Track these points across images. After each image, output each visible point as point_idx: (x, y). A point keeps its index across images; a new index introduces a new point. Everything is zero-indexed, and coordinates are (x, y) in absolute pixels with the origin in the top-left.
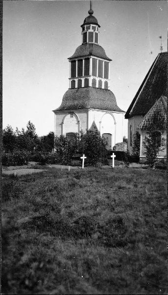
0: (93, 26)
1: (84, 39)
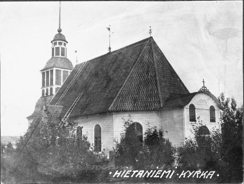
0: (59, 42)
1: (52, 51)
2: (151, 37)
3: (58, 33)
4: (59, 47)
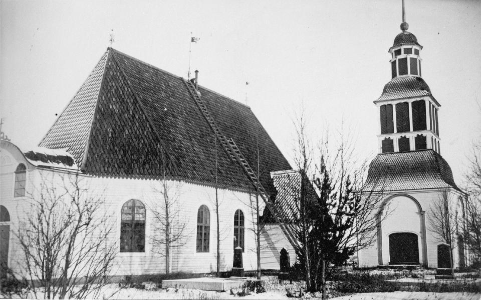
4: (416, 59)
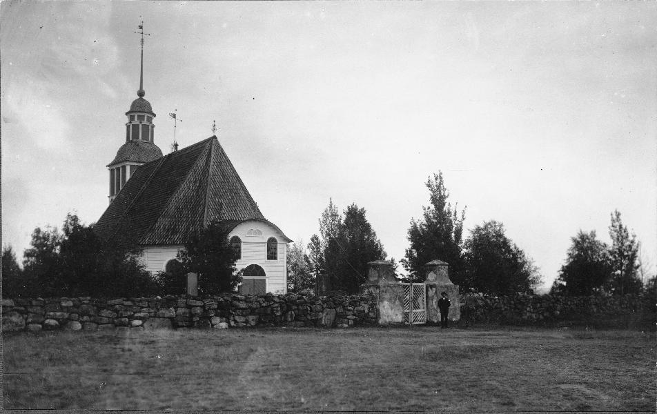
2: (215, 137)
3: (138, 97)
